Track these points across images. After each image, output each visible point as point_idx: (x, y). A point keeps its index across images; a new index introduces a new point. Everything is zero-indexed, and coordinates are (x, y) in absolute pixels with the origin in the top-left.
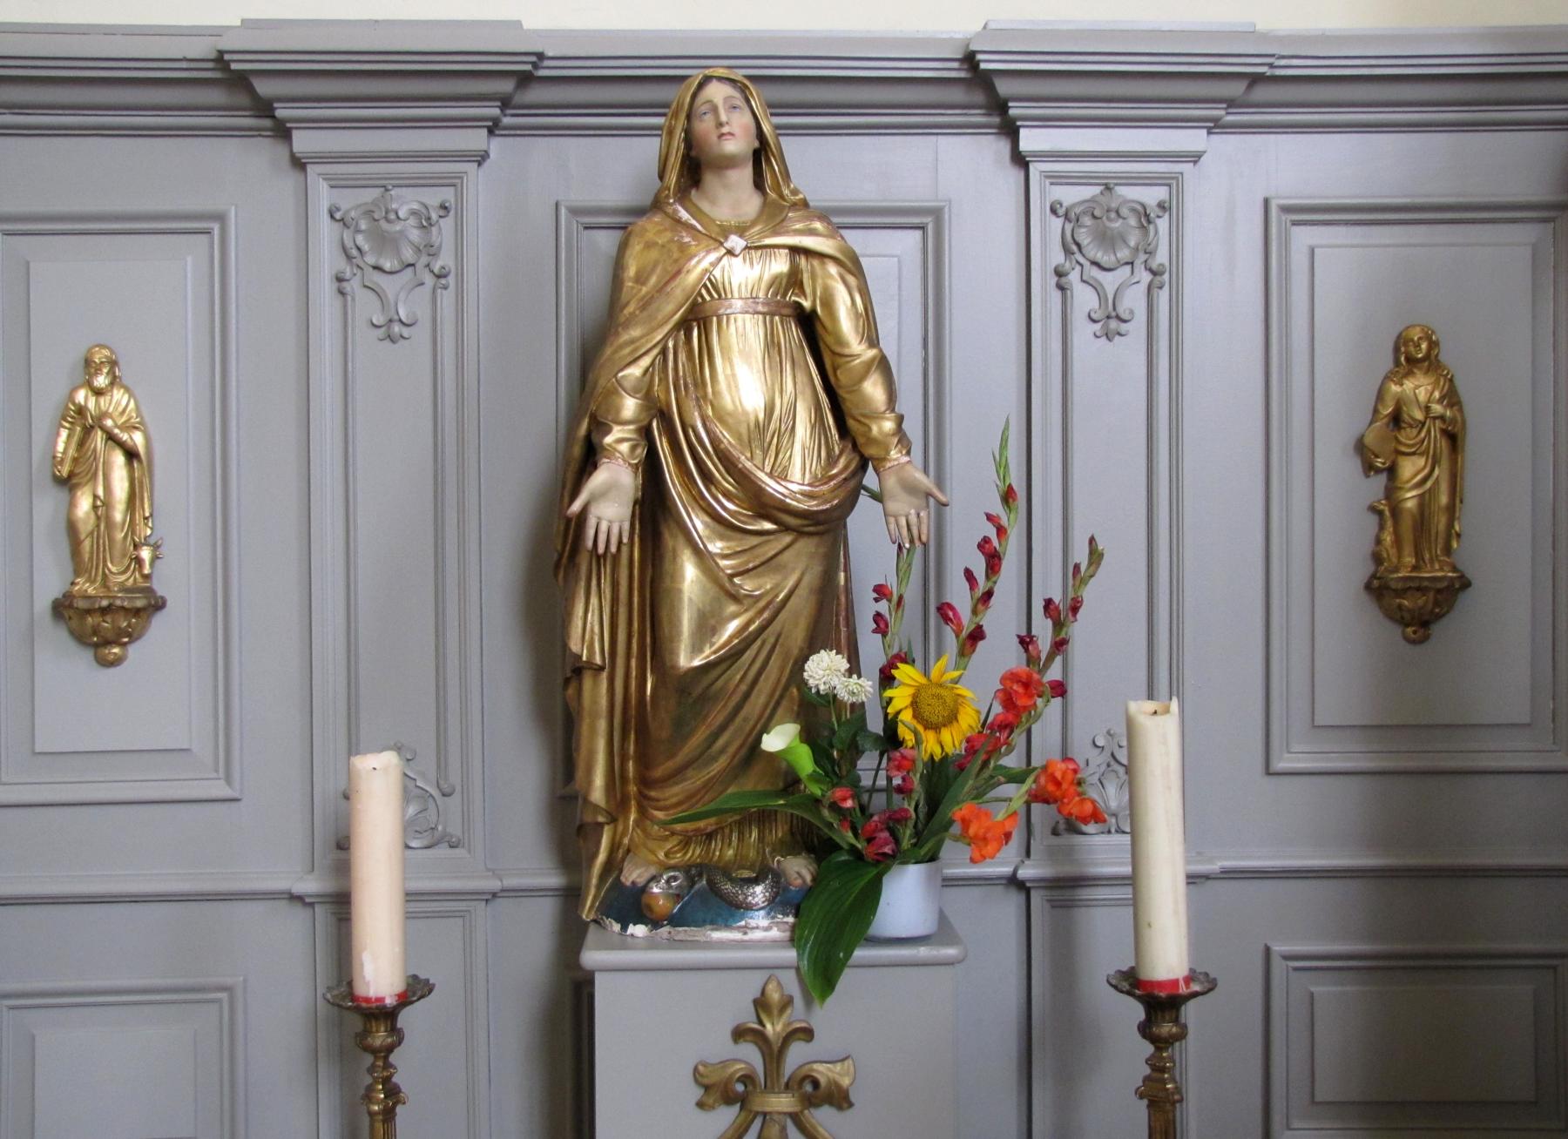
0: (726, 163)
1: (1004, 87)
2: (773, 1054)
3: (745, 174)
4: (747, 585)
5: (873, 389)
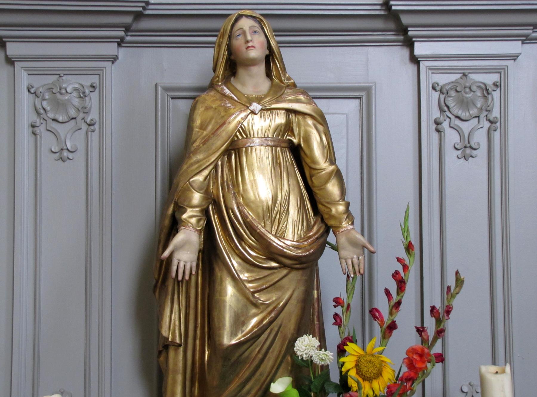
0: (251, 63)
1: (405, 20)
3: (261, 69)
4: (262, 298)
5: (333, 188)
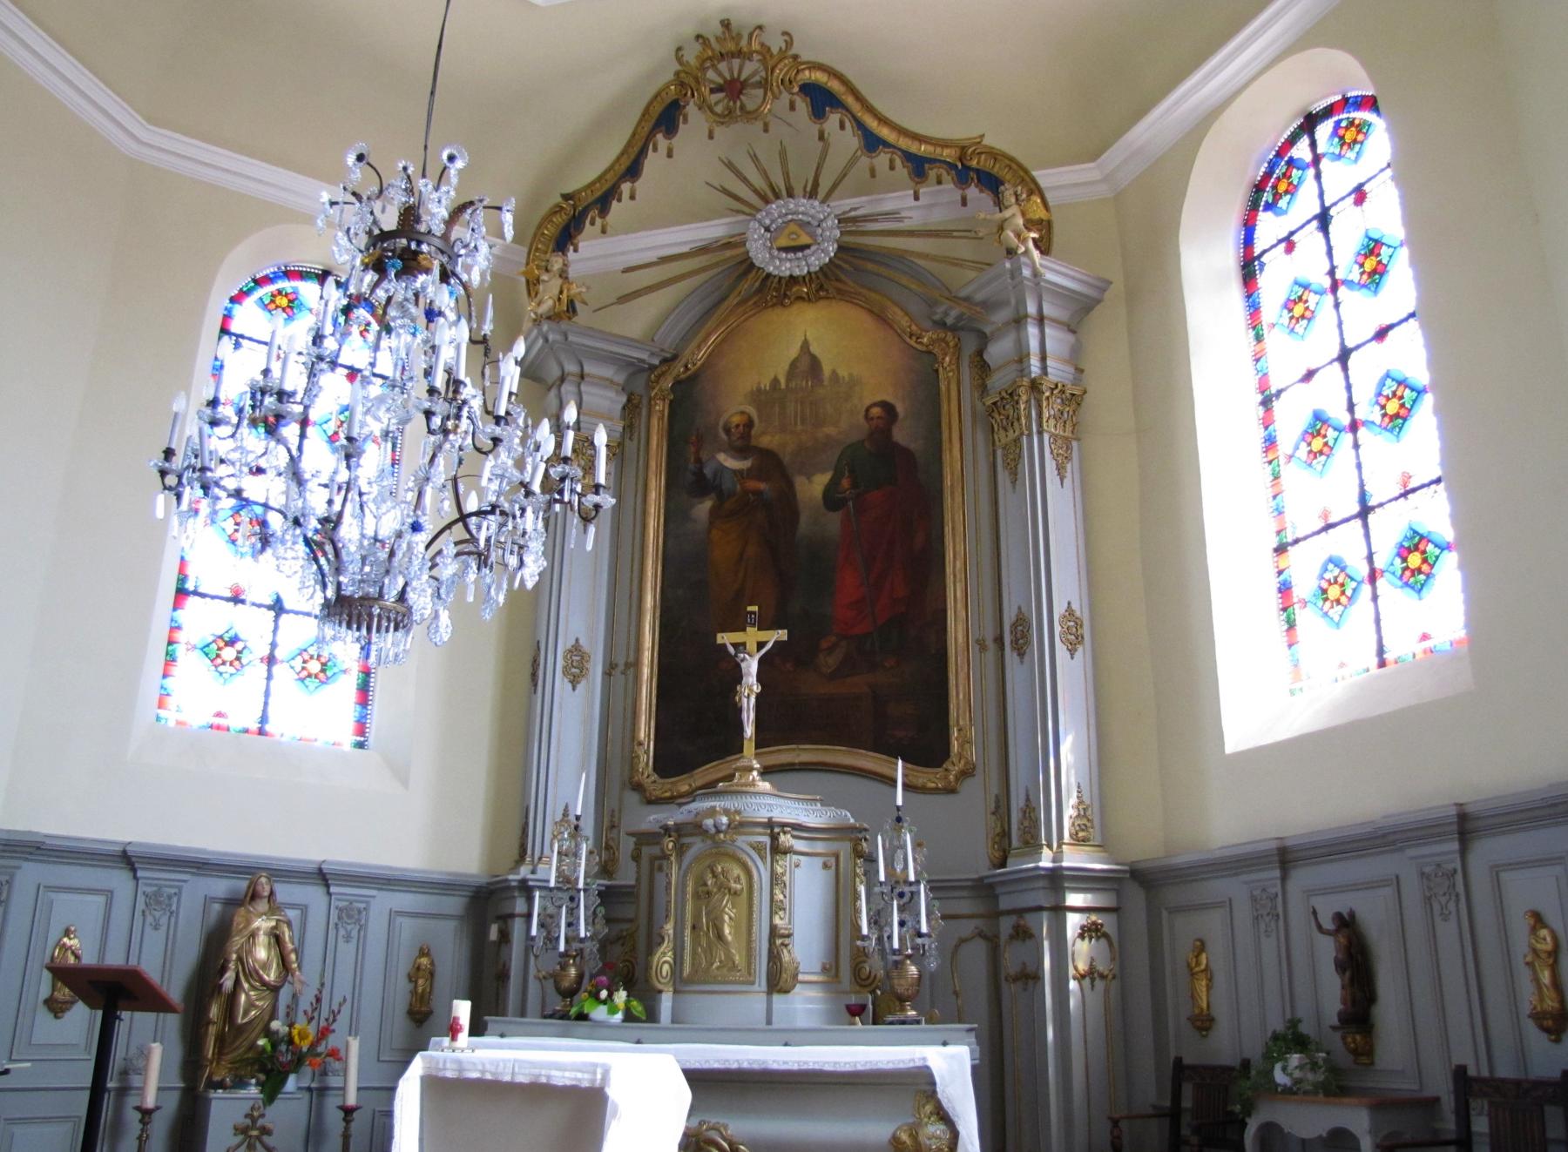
0: (261, 897)
1: (328, 877)
2: (254, 1120)
3: (266, 900)
4: (259, 1003)
5: (293, 957)
